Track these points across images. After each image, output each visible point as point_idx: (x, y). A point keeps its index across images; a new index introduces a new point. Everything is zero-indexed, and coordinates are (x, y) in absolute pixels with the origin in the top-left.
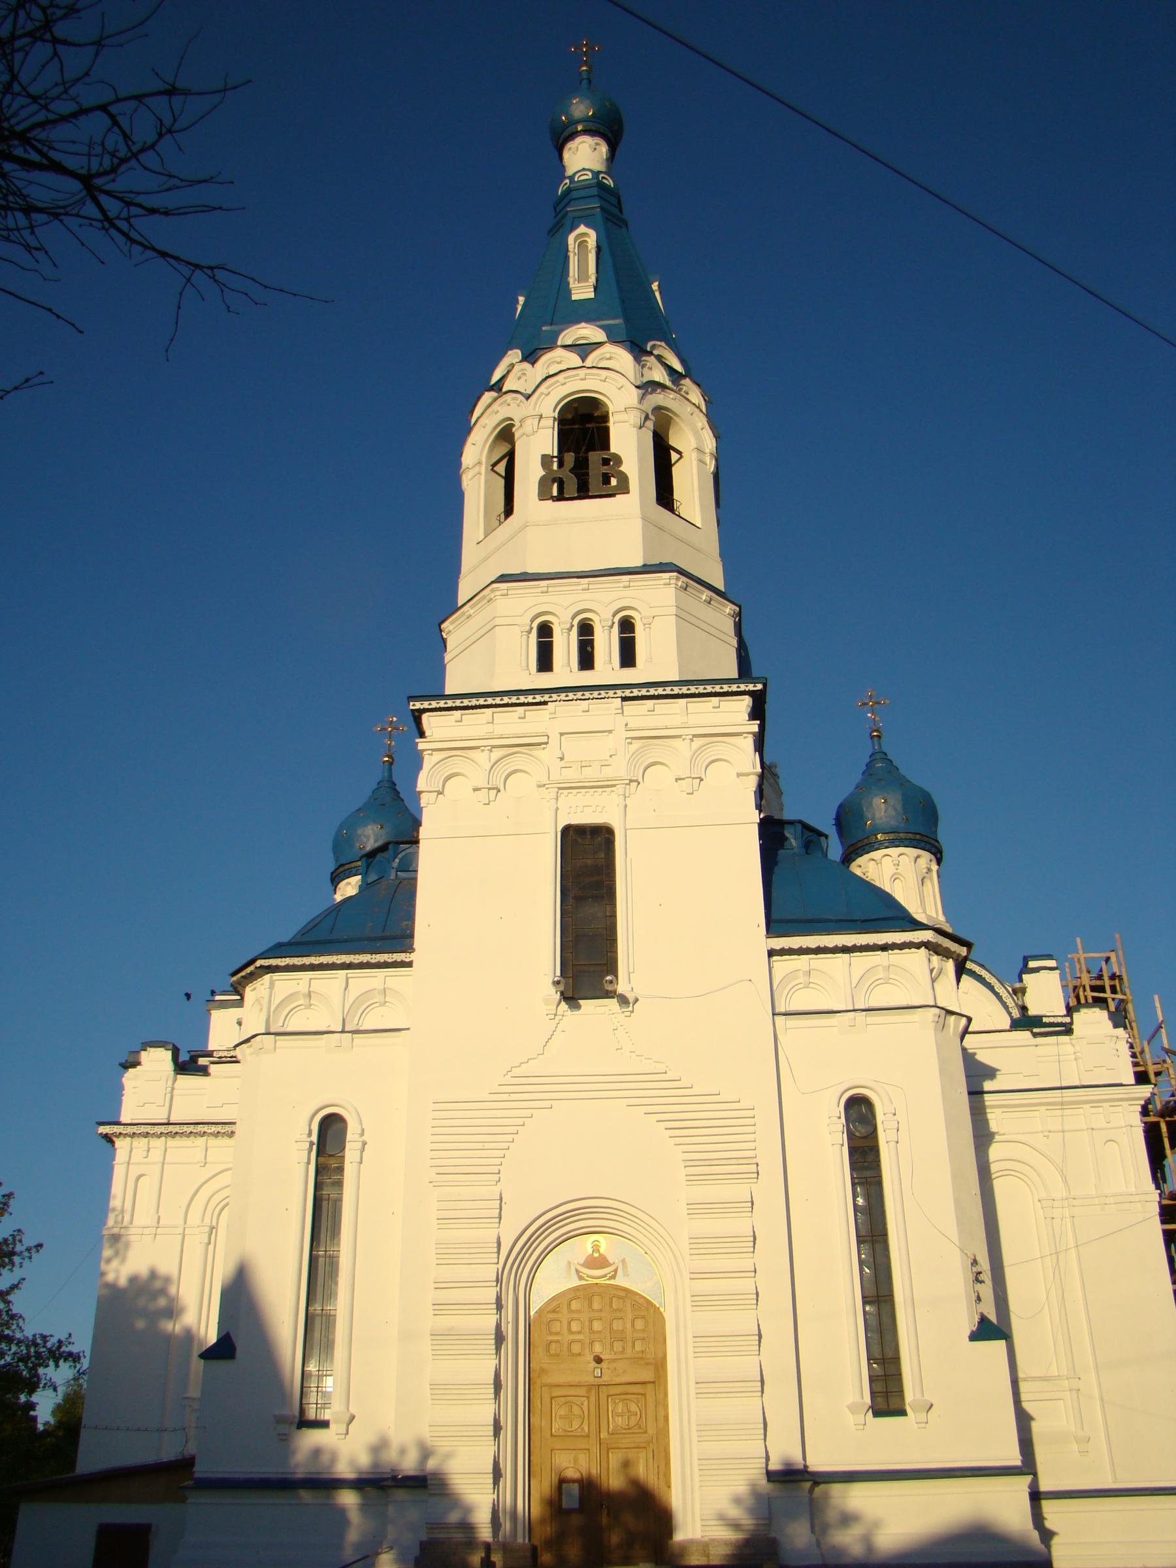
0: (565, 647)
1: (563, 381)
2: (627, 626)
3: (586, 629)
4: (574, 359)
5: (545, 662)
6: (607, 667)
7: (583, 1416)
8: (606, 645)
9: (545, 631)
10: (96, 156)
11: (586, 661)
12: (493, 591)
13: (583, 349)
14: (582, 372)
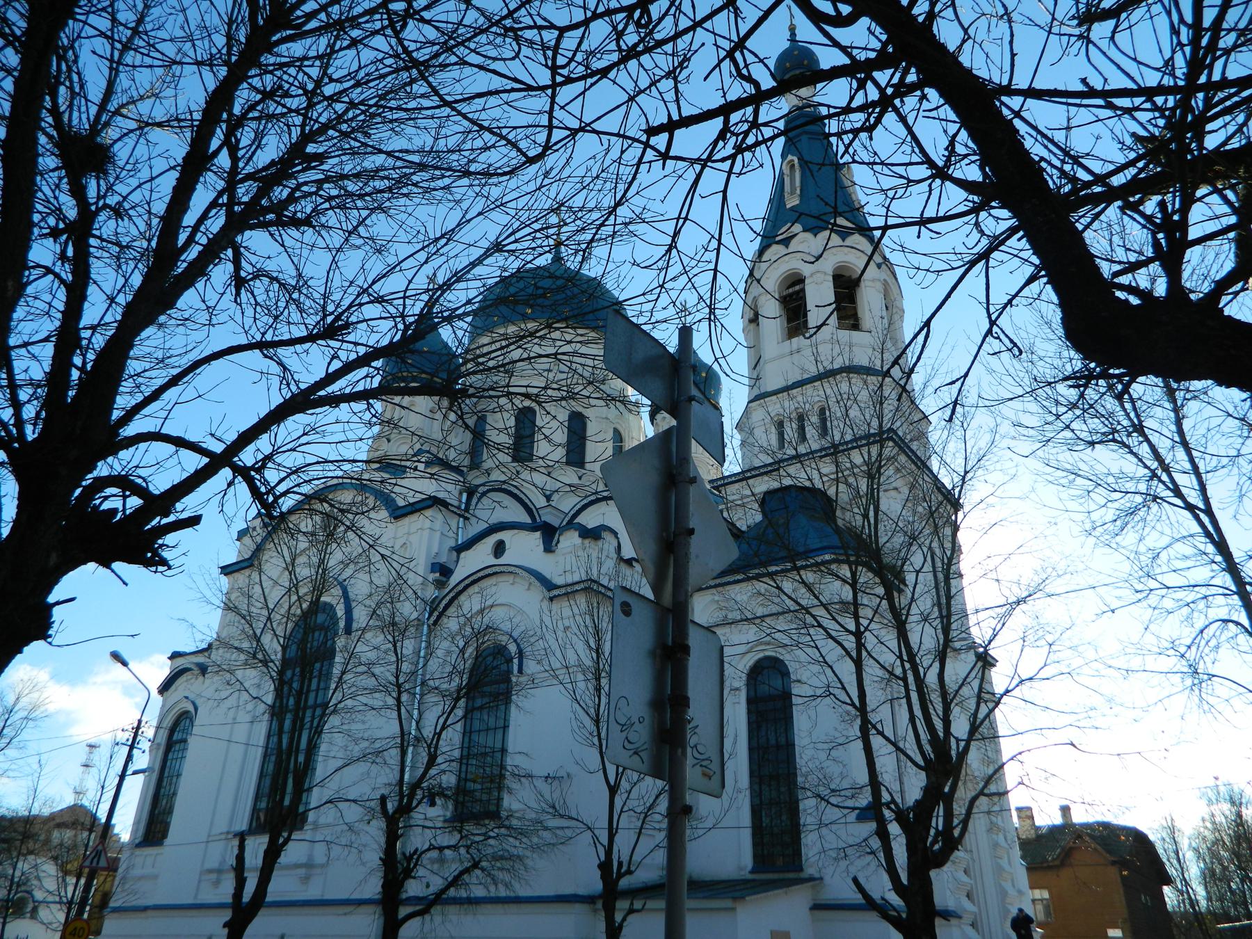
3: (801, 419)
13: (786, 242)
14: (786, 258)
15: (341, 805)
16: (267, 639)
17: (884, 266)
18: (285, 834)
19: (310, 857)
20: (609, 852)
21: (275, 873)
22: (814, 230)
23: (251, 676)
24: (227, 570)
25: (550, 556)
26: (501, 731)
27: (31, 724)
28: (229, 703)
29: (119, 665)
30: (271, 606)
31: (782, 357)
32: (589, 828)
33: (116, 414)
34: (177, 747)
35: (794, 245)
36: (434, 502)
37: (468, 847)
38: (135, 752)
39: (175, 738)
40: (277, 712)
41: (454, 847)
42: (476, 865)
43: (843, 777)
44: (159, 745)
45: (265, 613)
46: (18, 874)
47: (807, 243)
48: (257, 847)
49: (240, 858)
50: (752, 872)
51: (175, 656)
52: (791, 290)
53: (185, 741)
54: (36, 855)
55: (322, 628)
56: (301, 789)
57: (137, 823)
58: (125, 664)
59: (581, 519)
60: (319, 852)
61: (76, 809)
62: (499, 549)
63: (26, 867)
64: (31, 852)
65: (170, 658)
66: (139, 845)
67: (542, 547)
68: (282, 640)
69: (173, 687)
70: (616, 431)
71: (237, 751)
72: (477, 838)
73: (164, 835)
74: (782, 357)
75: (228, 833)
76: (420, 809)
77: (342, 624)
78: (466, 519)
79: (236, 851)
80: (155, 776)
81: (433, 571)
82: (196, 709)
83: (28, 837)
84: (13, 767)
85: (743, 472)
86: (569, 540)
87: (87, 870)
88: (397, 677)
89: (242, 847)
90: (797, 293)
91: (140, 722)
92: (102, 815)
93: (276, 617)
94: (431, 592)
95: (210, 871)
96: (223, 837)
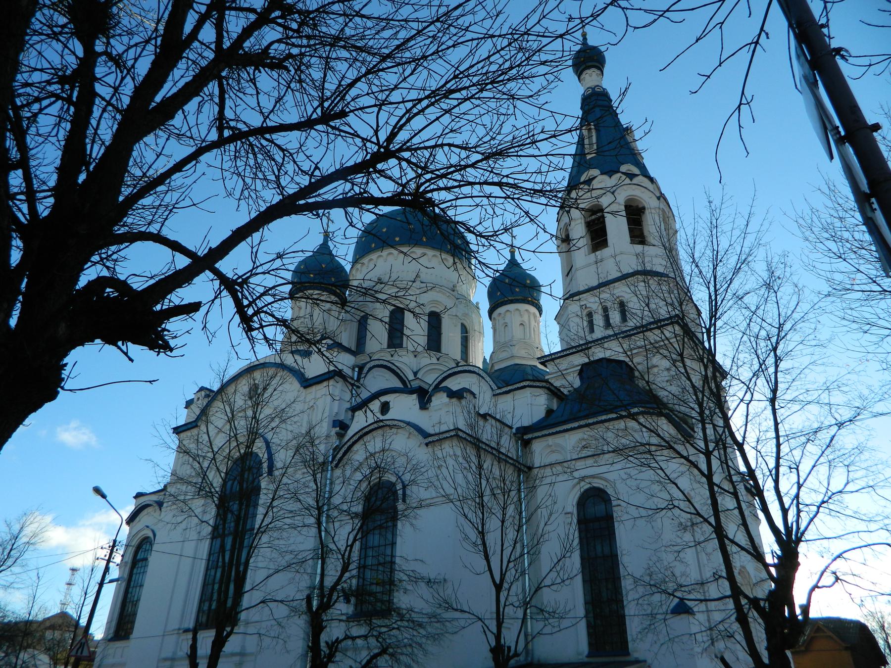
0: (599, 320)
3: (605, 310)
15: (271, 605)
16: (211, 475)
17: (661, 199)
18: (228, 629)
19: (243, 647)
20: (498, 637)
21: (220, 660)
22: (610, 173)
23: (198, 504)
24: (177, 430)
25: (424, 412)
26: (390, 547)
27: (31, 547)
28: (183, 525)
29: (99, 497)
30: (216, 449)
31: (589, 265)
32: (480, 619)
33: (126, 191)
37: (377, 638)
38: (111, 564)
39: (138, 557)
40: (217, 533)
41: (365, 637)
42: (384, 651)
43: (683, 574)
44: (126, 563)
45: (210, 455)
46: (20, 662)
47: (602, 181)
48: (206, 638)
49: (194, 647)
50: (588, 656)
51: (139, 495)
52: (593, 217)
53: (146, 559)
54: (34, 648)
55: (250, 469)
56: (239, 593)
57: (109, 623)
58: (104, 496)
59: (447, 383)
60: (251, 644)
61: (63, 615)
63: (26, 656)
64: (29, 646)
65: (135, 497)
66: (111, 640)
67: (418, 406)
68: (223, 475)
69: (137, 519)
70: (463, 326)
71: (187, 563)
72: (383, 630)
74: (589, 265)
75: (179, 629)
76: (337, 606)
77: (265, 465)
79: (190, 642)
80: (124, 585)
81: (334, 426)
82: (155, 535)
83: (28, 634)
84: (17, 580)
86: (440, 400)
87: (72, 660)
88: (317, 502)
89: (195, 639)
90: (598, 219)
91: (115, 541)
92: (83, 622)
93: (219, 458)
94: (335, 442)
95: (165, 659)
96: (176, 632)
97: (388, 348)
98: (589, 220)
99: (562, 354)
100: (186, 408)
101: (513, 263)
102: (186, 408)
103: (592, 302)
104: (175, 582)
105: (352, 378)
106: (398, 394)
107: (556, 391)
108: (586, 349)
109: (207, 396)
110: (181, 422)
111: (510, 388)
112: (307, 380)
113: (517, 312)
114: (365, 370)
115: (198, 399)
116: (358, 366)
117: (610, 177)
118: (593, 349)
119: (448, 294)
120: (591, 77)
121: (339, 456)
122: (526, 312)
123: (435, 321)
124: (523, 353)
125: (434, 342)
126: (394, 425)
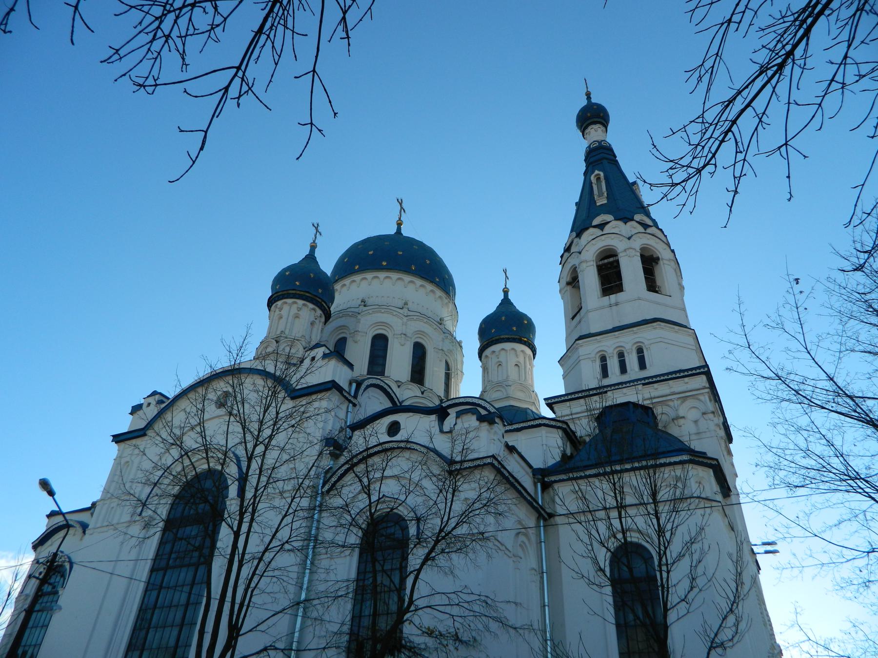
0: (613, 365)
1: (603, 239)
2: (640, 351)
3: (621, 355)
4: (598, 232)
5: (605, 372)
6: (633, 371)
7: (222, 386)
8: (632, 361)
9: (603, 359)
10: (187, 466)
11: (623, 369)
12: (577, 344)
13: (601, 226)
14: (603, 237)
22: (626, 219)
24: (118, 439)
29: (45, 493)
34: (45, 599)
35: (607, 229)
36: (332, 386)
44: (27, 596)
62: (394, 428)
65: (48, 516)
73: (732, 439)
78: (354, 405)
85: (566, 395)
90: (611, 263)
97: (368, 375)
98: (601, 263)
99: (566, 398)
100: (131, 414)
101: (506, 302)
102: (131, 414)
103: (609, 345)
104: (97, 617)
105: (349, 394)
106: (411, 414)
107: (571, 434)
108: (601, 393)
109: (160, 402)
110: (124, 429)
111: (522, 425)
112: (295, 390)
113: (513, 351)
114: (363, 387)
115: (149, 404)
116: (356, 381)
117: (626, 224)
118: (609, 394)
119: (435, 326)
120: (595, 133)
121: (334, 479)
122: (521, 353)
123: (419, 353)
124: (520, 395)
125: (418, 374)
126: (407, 446)
